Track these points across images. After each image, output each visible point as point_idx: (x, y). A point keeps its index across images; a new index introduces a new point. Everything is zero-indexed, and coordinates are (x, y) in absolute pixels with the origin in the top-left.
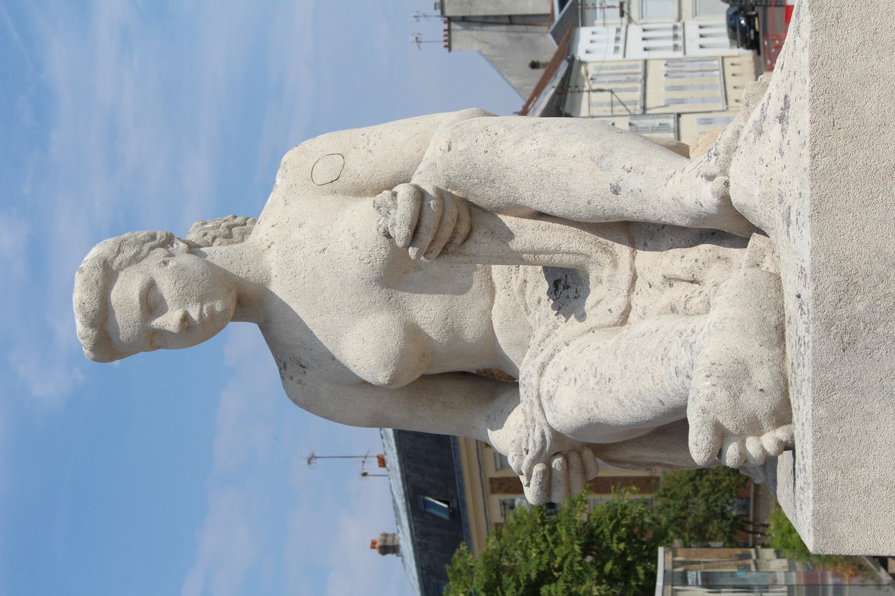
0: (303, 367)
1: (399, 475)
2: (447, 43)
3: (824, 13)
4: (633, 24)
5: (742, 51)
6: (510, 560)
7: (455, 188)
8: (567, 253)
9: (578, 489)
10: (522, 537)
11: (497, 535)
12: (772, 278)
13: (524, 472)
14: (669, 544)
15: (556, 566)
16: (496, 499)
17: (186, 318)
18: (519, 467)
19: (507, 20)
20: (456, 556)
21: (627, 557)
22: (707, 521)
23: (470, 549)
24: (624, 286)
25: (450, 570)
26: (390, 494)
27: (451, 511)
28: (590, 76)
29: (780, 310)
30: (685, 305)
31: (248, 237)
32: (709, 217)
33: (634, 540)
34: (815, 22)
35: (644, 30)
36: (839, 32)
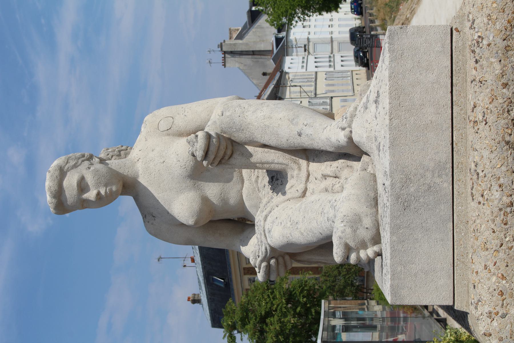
0: (154, 217)
1: (201, 266)
2: (223, 64)
3: (395, 53)
4: (310, 55)
5: (361, 68)
7: (225, 133)
8: (277, 164)
9: (283, 274)
10: (258, 296)
11: (246, 295)
12: (372, 176)
13: (257, 266)
14: (327, 298)
15: (274, 309)
16: (246, 277)
17: (99, 194)
18: (255, 264)
19: (252, 53)
20: (227, 305)
21: (307, 305)
22: (345, 287)
23: (234, 301)
24: (304, 179)
25: (224, 311)
27: (225, 283)
28: (290, 79)
29: (376, 191)
30: (332, 188)
31: (128, 156)
32: (343, 147)
33: (310, 297)
34: (391, 57)
35: (315, 58)
36: (402, 62)
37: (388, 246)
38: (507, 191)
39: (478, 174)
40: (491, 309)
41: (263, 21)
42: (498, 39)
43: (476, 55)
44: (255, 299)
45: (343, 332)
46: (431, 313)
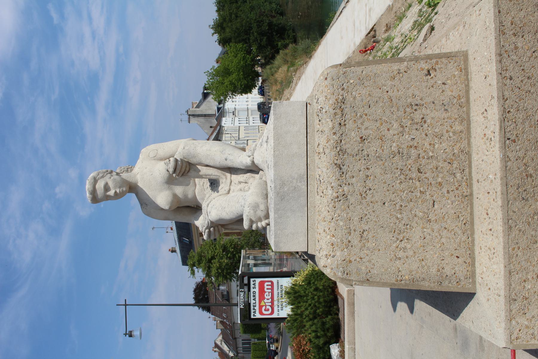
6: (204, 254)
7: (185, 159)
17: (116, 192)
18: (202, 230)
20: (190, 253)
22: (255, 243)
23: (194, 251)
24: (229, 184)
26: (173, 237)
29: (267, 190)
32: (249, 166)
37: (273, 220)
38: (335, 190)
39: (320, 181)
40: (327, 253)
41: (210, 98)
42: (331, 109)
43: (319, 117)
44: (205, 250)
45: (254, 267)
46: (300, 256)
